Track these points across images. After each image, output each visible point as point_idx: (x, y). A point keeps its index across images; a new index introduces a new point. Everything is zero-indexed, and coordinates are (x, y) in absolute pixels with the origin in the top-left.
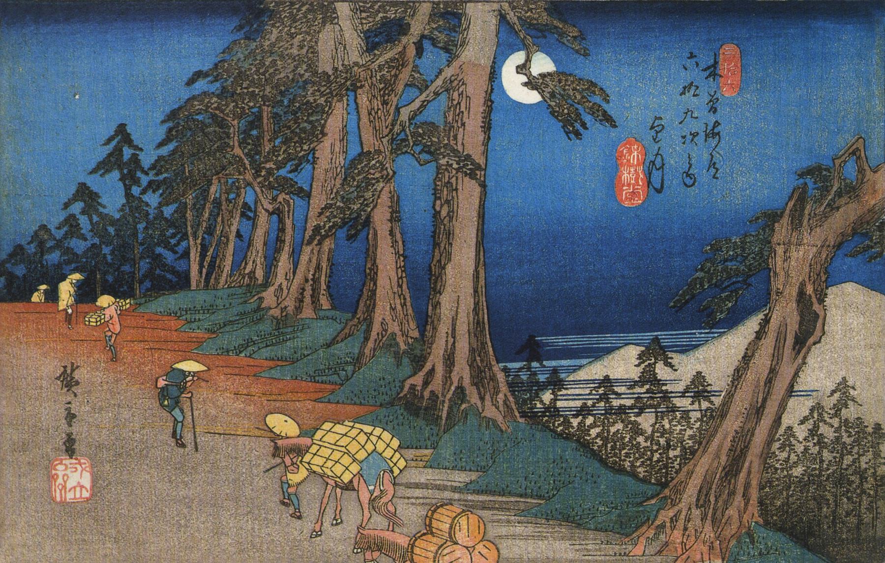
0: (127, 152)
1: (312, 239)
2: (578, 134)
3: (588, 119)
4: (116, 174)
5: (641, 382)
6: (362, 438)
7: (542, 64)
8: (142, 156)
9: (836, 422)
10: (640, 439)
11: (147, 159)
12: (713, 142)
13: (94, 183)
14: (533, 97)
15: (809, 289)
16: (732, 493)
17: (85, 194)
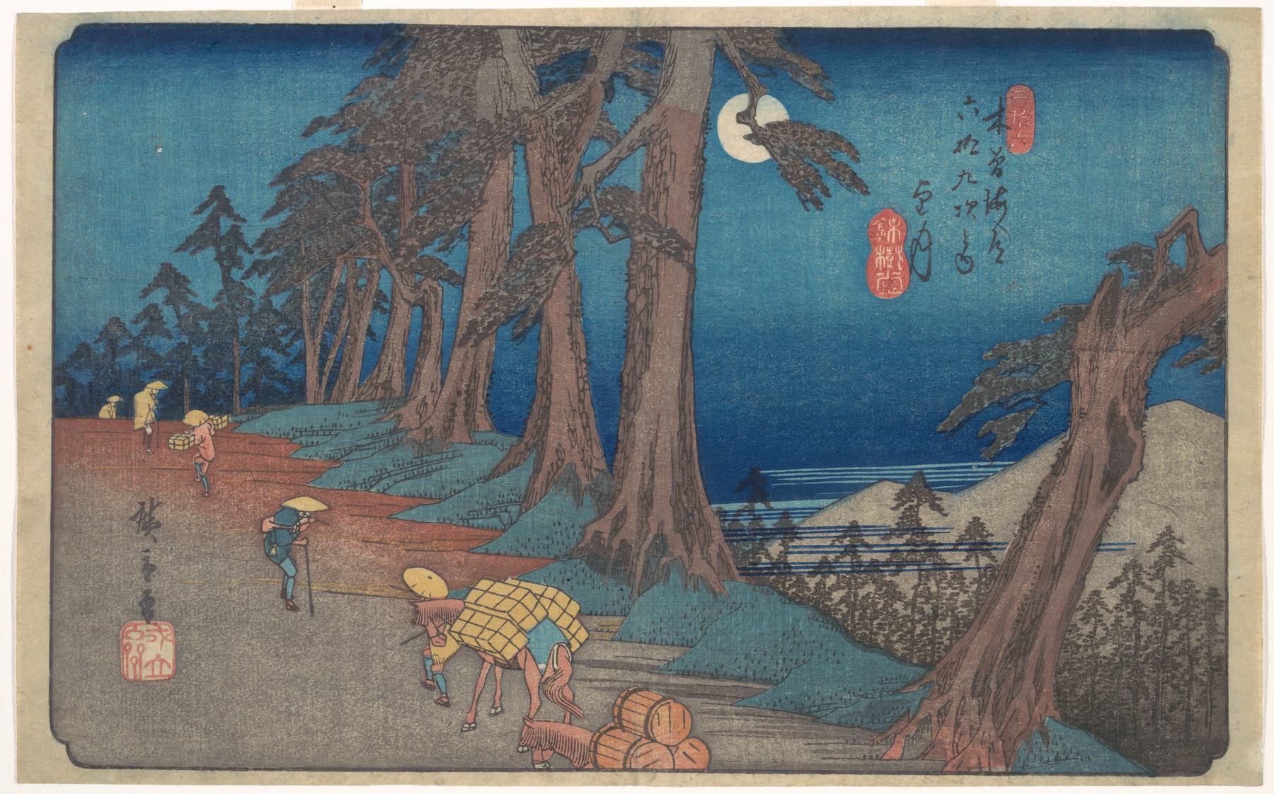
0: (225, 224)
1: (466, 337)
2: (818, 204)
3: (830, 182)
4: (210, 252)
5: (900, 530)
6: (530, 601)
7: (771, 111)
10: (898, 605)
11: (251, 234)
12: (996, 214)
13: (181, 263)
14: (757, 154)
15: (1124, 410)
16: (1020, 678)
17: (171, 278)
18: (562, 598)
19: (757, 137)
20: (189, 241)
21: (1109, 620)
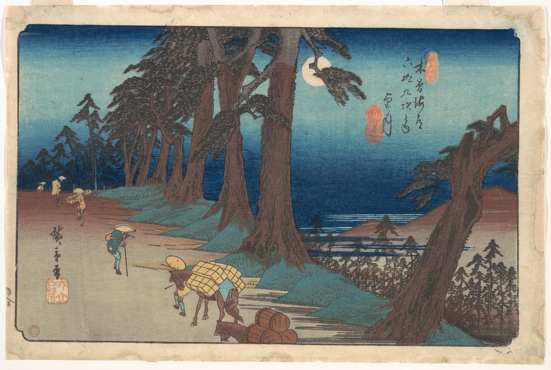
0: (91, 110)
2: (343, 103)
3: (349, 93)
7: (324, 63)
8: (99, 112)
9: (488, 265)
12: (419, 108)
14: (319, 82)
18: (234, 270)
19: (319, 74)
20: (76, 117)
21: (467, 280)
